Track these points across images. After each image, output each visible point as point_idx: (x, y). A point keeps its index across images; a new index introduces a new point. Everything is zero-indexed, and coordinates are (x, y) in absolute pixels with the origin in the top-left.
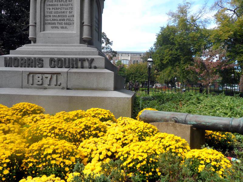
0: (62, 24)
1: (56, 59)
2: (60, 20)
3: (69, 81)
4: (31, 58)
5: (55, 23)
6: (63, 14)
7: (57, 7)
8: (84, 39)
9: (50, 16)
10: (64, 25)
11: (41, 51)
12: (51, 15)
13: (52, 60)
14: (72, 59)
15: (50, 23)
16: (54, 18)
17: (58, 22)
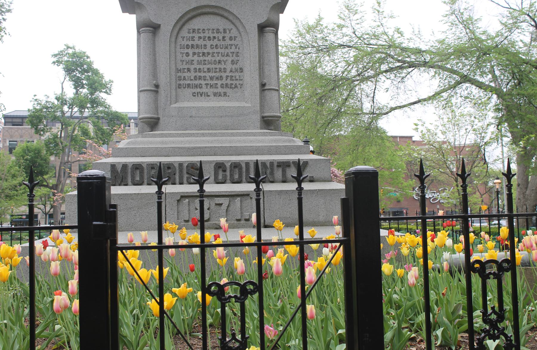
0: (217, 88)
1: (228, 165)
2: (211, 78)
3: (268, 211)
4: (172, 164)
5: (201, 84)
6: (218, 66)
7: (205, 51)
8: (265, 119)
9: (189, 70)
10: (220, 90)
11: (184, 148)
12: (192, 67)
13: (219, 166)
14: (264, 164)
15: (189, 85)
16: (198, 74)
17: (206, 82)
